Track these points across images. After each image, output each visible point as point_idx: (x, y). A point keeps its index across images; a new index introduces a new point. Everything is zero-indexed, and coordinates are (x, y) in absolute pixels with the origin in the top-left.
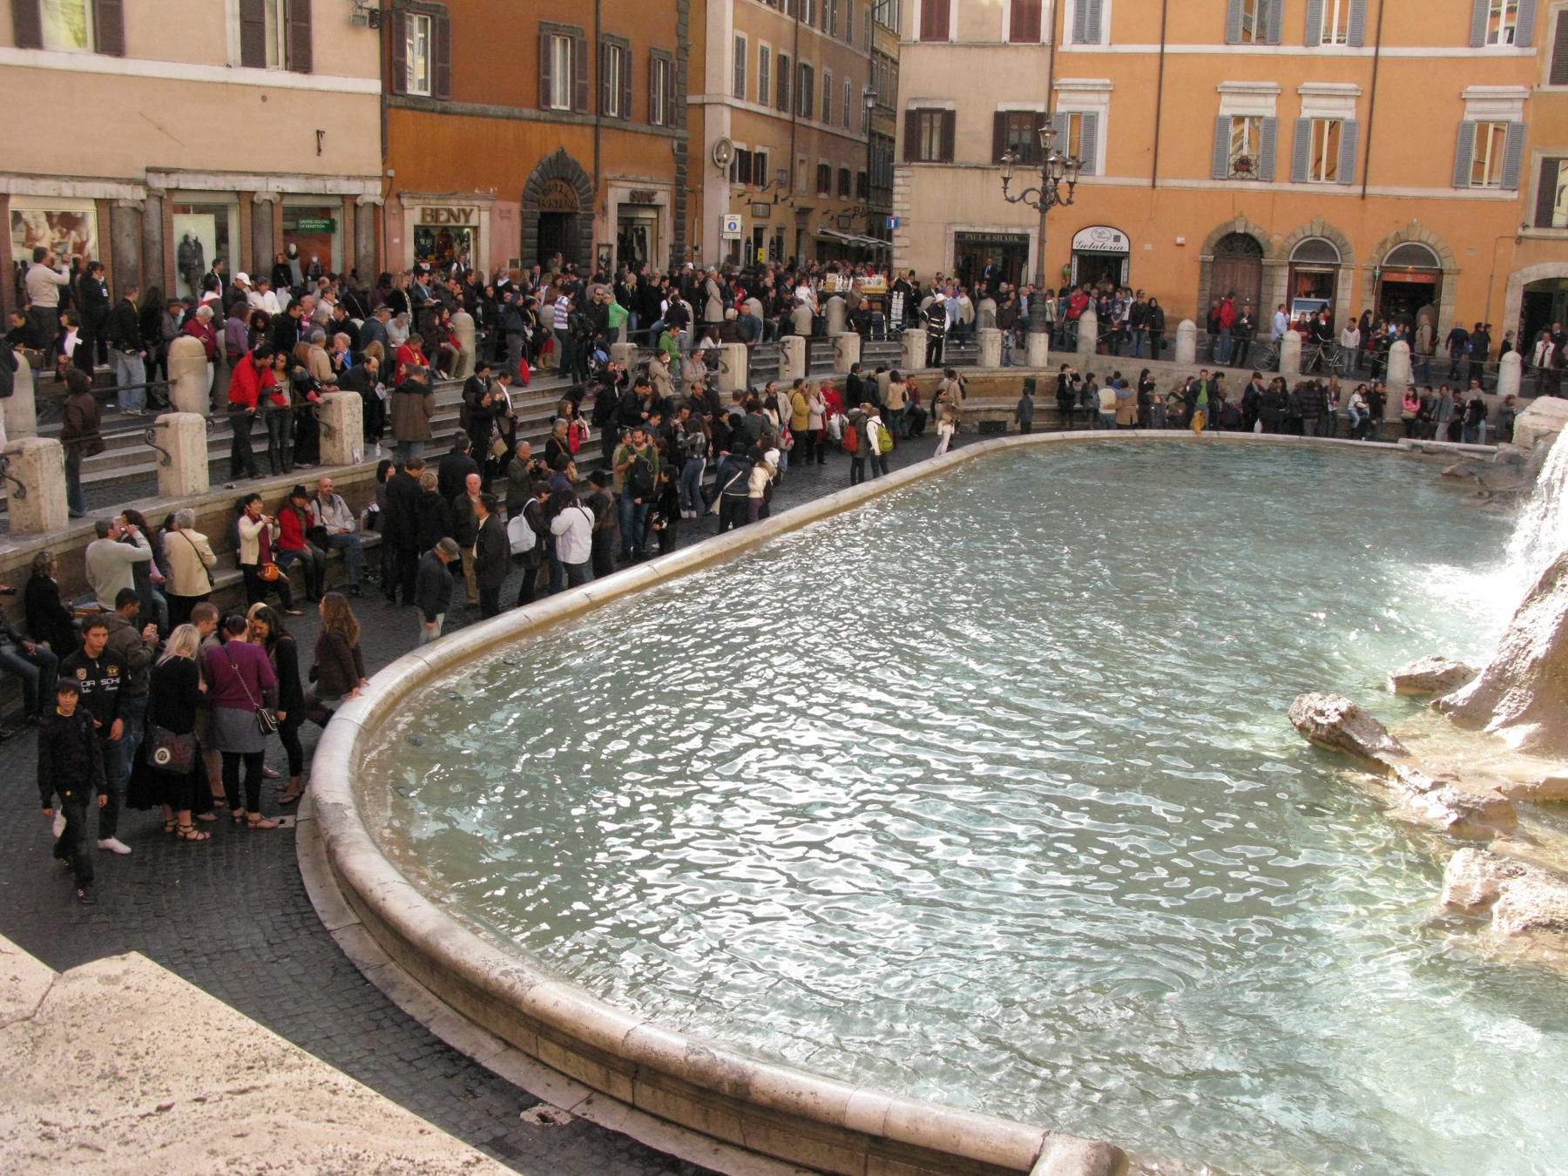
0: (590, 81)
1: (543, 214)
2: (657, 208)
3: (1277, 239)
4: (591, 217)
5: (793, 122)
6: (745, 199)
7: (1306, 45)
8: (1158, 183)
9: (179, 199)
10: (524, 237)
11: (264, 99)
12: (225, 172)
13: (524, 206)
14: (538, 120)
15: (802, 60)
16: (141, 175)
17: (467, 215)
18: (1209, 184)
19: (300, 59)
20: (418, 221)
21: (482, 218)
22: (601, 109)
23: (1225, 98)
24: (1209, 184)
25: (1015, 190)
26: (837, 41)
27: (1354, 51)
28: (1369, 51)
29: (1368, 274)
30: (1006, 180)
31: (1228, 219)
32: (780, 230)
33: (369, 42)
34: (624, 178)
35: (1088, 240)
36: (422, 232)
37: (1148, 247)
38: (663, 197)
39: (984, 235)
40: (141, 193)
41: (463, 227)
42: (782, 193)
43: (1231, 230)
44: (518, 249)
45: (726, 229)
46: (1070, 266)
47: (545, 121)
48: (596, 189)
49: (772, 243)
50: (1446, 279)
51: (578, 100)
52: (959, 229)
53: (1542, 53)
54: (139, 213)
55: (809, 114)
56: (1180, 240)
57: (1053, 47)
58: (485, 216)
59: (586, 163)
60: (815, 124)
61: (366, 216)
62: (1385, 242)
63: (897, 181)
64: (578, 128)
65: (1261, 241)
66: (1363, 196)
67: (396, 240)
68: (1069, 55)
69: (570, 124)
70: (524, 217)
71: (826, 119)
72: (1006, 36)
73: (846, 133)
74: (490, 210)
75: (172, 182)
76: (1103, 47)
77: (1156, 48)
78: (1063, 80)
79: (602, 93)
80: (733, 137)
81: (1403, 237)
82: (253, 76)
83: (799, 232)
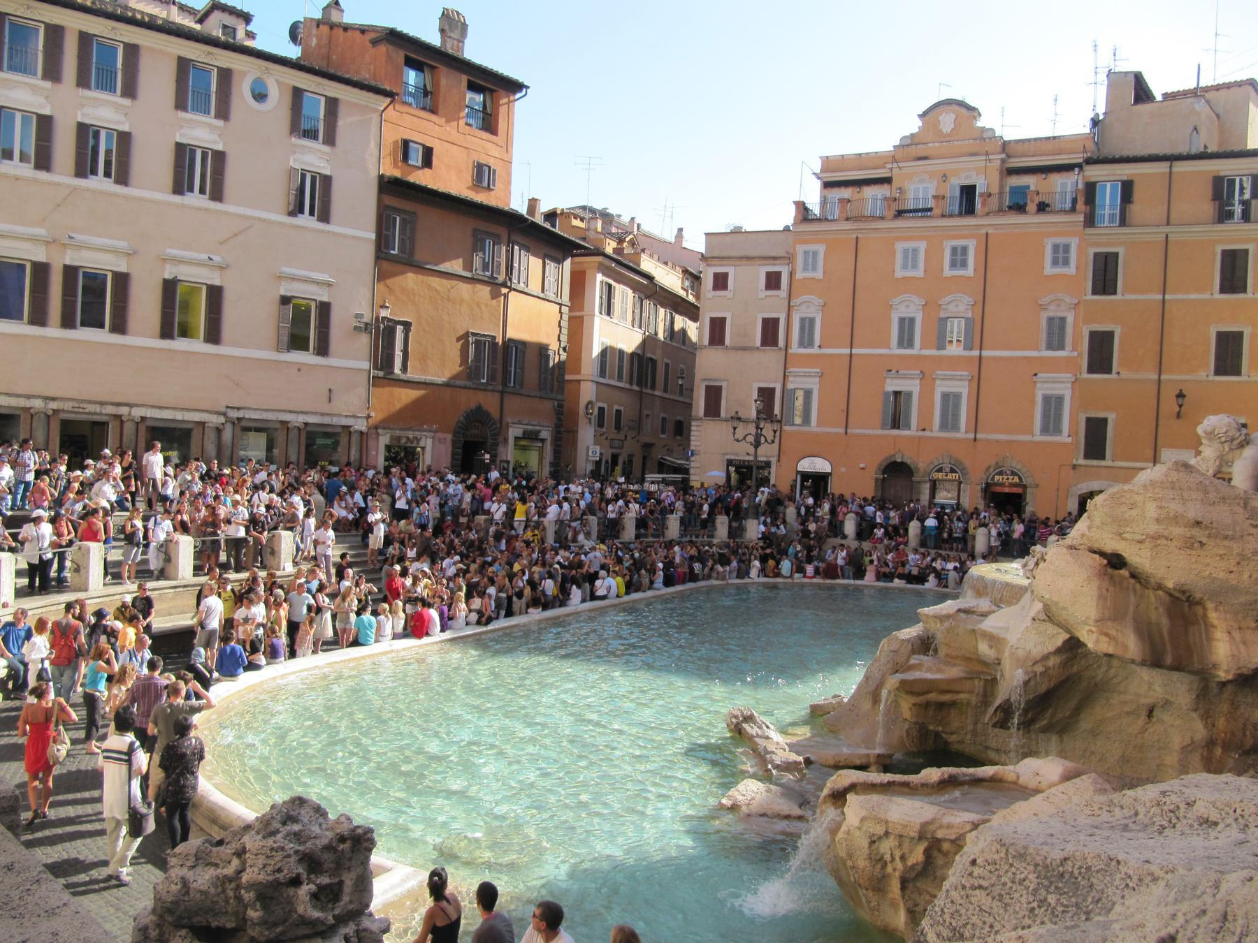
0: (499, 367)
1: (466, 442)
2: (543, 440)
3: (922, 466)
4: (497, 445)
5: (641, 392)
6: (604, 437)
7: (938, 349)
8: (849, 431)
9: (244, 424)
10: (453, 454)
11: (299, 370)
12: (273, 410)
13: (454, 436)
14: (465, 388)
15: (649, 355)
16: (223, 410)
17: (418, 440)
18: (880, 432)
19: (323, 350)
20: (388, 443)
21: (427, 443)
22: (505, 384)
23: (938, 382)
24: (880, 432)
25: (739, 434)
26: (674, 344)
27: (967, 353)
28: (976, 353)
29: (979, 487)
30: (735, 429)
31: (892, 452)
32: (631, 456)
33: (364, 340)
34: (520, 423)
35: (806, 465)
36: (388, 448)
37: (843, 470)
38: (545, 434)
39: (744, 461)
40: (222, 420)
41: (416, 447)
42: (633, 433)
43: (893, 460)
44: (449, 461)
45: (590, 454)
46: (796, 481)
47: (470, 388)
48: (501, 428)
49: (624, 463)
50: (1029, 490)
51: (492, 378)
52: (729, 457)
53: (1080, 355)
54: (219, 431)
55: (653, 387)
56: (862, 466)
57: (786, 349)
58: (429, 441)
59: (495, 413)
60: (657, 393)
61: (355, 438)
62: (989, 467)
63: (693, 428)
64: (489, 393)
65: (913, 467)
66: (975, 439)
67: (374, 453)
68: (796, 355)
69: (485, 390)
70: (454, 443)
71: (666, 390)
72: (758, 343)
73: (681, 399)
74: (433, 438)
75: (240, 414)
76: (915, 351)
77: (847, 351)
78: (791, 370)
79: (506, 372)
80: (598, 400)
81: (1001, 464)
82: (297, 357)
83: (645, 458)
